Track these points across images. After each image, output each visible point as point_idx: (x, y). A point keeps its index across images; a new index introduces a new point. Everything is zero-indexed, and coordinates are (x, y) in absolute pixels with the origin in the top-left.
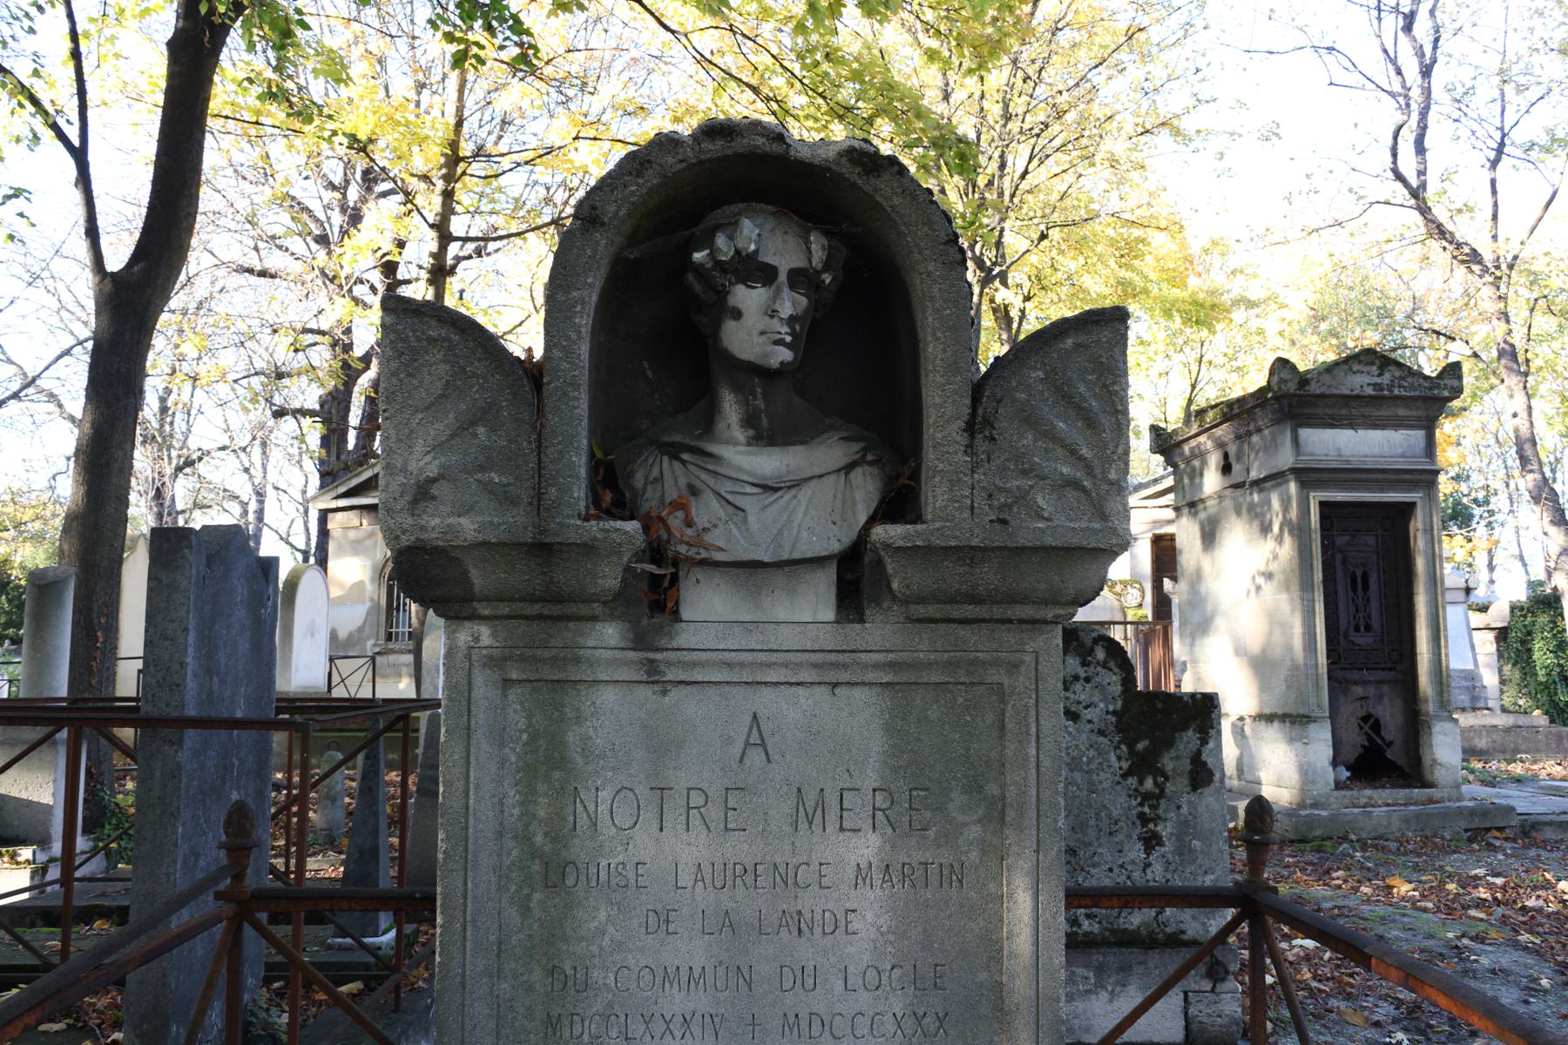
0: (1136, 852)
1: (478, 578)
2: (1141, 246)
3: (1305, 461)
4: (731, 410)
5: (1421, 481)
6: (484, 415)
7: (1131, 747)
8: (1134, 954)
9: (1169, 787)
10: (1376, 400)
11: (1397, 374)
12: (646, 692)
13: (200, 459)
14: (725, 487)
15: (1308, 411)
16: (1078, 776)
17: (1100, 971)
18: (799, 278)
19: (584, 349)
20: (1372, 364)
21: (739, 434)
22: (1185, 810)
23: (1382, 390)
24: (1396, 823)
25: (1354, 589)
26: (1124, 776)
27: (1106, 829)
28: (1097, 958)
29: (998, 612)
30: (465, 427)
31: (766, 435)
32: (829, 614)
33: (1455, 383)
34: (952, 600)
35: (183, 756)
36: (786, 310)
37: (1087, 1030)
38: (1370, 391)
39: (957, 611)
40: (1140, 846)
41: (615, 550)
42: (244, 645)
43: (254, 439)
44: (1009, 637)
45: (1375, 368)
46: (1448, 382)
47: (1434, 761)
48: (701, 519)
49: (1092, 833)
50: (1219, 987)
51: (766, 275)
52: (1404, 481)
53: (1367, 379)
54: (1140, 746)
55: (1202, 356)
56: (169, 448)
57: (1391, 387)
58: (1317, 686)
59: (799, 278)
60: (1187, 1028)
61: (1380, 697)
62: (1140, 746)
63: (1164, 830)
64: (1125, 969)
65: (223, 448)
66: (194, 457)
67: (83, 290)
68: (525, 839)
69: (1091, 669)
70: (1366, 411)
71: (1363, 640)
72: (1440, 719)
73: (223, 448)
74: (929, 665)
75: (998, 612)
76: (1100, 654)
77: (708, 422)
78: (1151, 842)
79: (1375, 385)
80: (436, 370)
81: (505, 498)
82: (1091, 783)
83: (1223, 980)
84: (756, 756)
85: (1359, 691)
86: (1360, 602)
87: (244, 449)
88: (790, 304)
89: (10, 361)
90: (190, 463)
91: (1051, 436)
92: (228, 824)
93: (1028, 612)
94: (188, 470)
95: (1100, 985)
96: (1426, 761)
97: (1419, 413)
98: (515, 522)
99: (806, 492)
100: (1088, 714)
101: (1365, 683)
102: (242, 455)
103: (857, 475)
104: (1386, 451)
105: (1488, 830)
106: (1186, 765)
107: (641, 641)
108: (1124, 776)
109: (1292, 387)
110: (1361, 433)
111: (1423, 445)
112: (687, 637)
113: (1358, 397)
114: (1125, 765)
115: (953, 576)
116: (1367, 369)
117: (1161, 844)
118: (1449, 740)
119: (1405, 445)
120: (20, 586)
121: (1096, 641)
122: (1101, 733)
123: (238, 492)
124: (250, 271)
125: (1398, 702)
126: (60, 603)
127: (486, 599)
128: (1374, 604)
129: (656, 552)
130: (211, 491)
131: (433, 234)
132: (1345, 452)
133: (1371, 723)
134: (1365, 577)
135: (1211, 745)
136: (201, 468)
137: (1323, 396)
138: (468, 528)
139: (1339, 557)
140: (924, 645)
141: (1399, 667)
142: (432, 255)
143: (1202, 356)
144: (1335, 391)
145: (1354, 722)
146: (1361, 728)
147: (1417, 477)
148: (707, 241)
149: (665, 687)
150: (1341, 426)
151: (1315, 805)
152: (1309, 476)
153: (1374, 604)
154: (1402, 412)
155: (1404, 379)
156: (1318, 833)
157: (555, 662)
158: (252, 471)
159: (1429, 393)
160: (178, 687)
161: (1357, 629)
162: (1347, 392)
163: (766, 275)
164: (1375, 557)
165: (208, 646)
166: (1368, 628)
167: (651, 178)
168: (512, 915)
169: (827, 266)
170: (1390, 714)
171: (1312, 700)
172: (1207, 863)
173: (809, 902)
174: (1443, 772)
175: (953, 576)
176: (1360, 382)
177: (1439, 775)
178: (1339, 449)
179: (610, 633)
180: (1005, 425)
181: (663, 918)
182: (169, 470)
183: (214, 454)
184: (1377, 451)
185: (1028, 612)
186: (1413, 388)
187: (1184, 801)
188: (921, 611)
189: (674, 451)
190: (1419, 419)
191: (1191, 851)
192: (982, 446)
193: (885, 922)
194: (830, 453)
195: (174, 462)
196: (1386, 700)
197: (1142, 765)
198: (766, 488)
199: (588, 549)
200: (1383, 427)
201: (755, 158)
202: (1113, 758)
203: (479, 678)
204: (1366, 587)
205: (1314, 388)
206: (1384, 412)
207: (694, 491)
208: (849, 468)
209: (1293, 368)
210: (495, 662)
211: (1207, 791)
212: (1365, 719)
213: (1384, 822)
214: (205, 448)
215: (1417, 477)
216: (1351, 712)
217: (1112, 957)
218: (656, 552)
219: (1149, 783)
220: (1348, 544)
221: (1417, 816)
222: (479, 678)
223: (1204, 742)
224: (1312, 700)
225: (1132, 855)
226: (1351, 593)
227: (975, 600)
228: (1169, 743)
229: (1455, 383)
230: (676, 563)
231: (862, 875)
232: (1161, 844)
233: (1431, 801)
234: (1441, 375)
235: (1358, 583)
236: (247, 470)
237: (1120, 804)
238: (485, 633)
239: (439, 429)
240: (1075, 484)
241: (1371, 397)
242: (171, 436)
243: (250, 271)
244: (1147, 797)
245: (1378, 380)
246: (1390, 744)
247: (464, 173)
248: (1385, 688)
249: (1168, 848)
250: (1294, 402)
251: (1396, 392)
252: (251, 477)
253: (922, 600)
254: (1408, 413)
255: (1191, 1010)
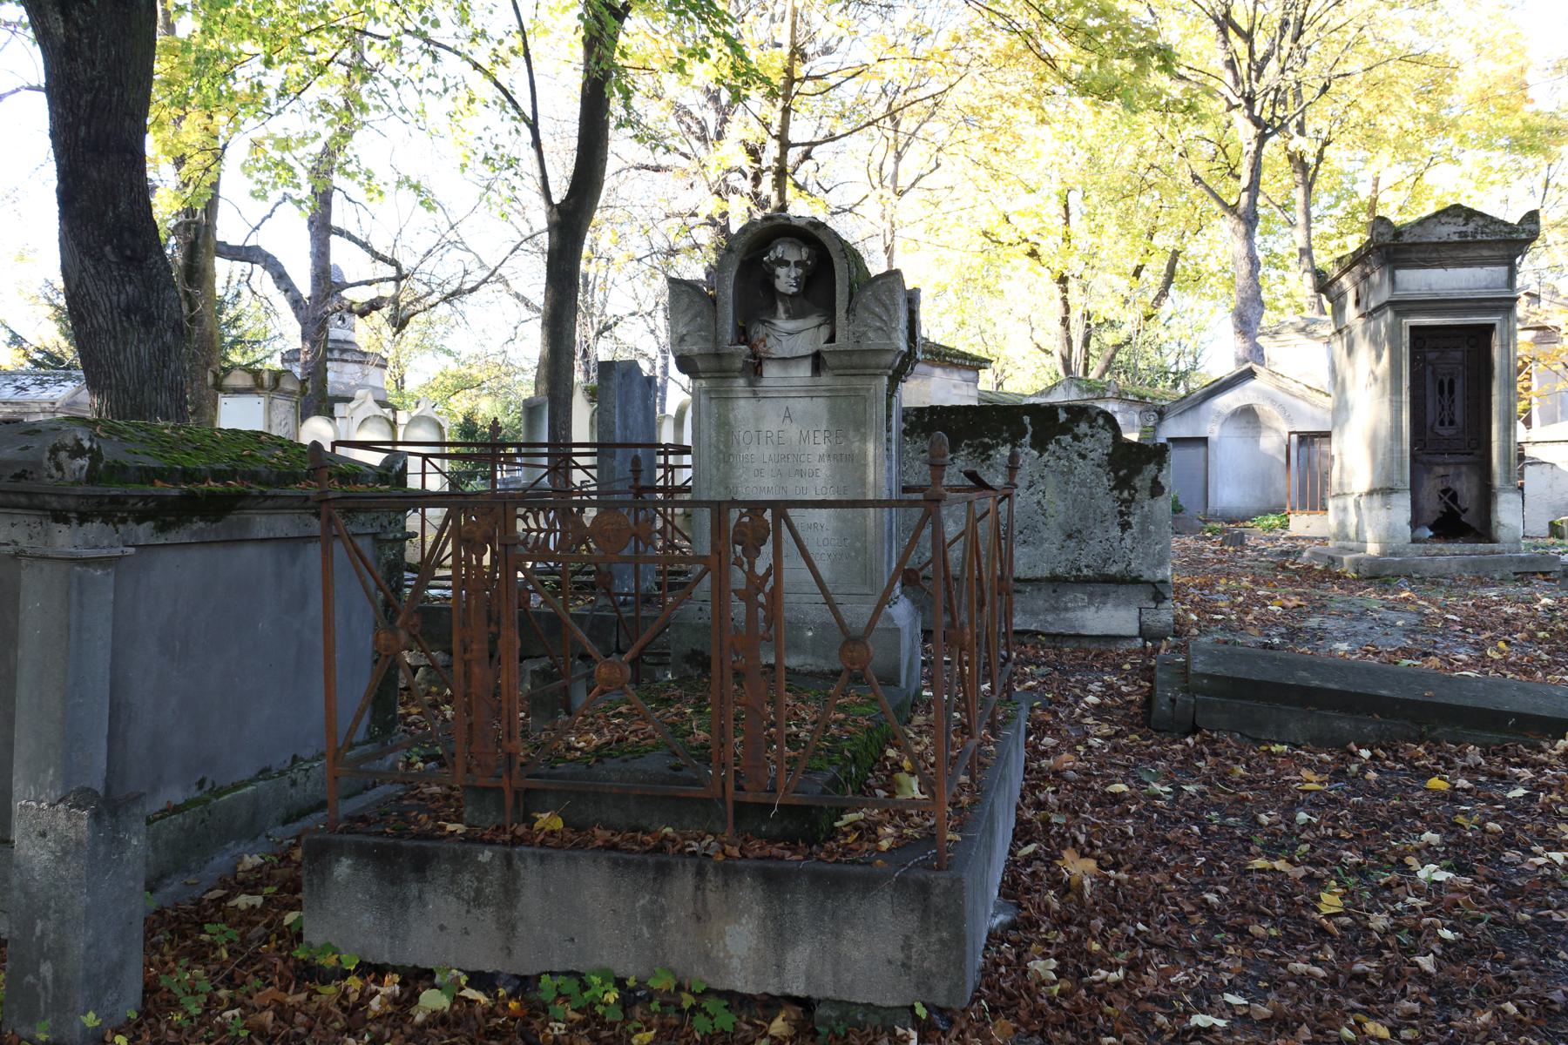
0: (1117, 532)
1: (700, 365)
2: (1447, 80)
3: (1400, 295)
4: (781, 308)
5: (1501, 307)
6: (699, 314)
7: (1116, 473)
8: (1112, 587)
9: (1137, 496)
10: (1463, 244)
11: (1481, 223)
12: (753, 401)
13: (616, 324)
14: (777, 334)
15: (1403, 256)
16: (1084, 490)
17: (1091, 595)
18: (797, 264)
19: (730, 292)
20: (1460, 216)
21: (783, 316)
22: (1146, 509)
23: (1466, 236)
24: (1454, 567)
25: (1441, 392)
26: (1111, 490)
27: (1099, 519)
28: (1090, 588)
29: (861, 372)
30: (694, 318)
31: (792, 316)
32: (809, 374)
33: (1533, 227)
34: (846, 368)
35: (616, 463)
36: (793, 275)
37: (1083, 627)
38: (1455, 238)
39: (848, 372)
40: (1118, 528)
41: (740, 355)
42: (640, 418)
43: (657, 304)
44: (867, 381)
45: (1461, 219)
46: (1527, 227)
47: (1499, 523)
48: (769, 345)
49: (1091, 521)
50: (1160, 606)
51: (787, 264)
52: (1486, 307)
53: (1453, 229)
54: (1121, 473)
55: (1548, 181)
56: (592, 315)
57: (1474, 234)
58: (1401, 466)
59: (797, 264)
60: (1140, 628)
61: (1459, 475)
62: (1121, 473)
63: (1133, 520)
64: (1106, 595)
65: (633, 314)
66: (611, 322)
67: (540, 220)
68: (717, 448)
69: (1095, 430)
70: (1454, 254)
71: (1446, 432)
72: (1505, 491)
73: (633, 314)
74: (841, 390)
75: (861, 372)
76: (1101, 421)
77: (774, 314)
78: (1125, 526)
79: (1460, 233)
80: (685, 300)
81: (706, 339)
82: (1091, 494)
83: (1162, 602)
84: (788, 420)
85: (1441, 470)
86: (1446, 403)
87: (650, 314)
88: (795, 272)
89: (468, 250)
90: (607, 328)
91: (874, 313)
92: (633, 462)
93: (871, 371)
94: (605, 334)
95: (1091, 603)
96: (1494, 524)
97: (1502, 253)
98: (707, 347)
99: (803, 334)
100: (1091, 455)
101: (1446, 464)
102: (648, 318)
103: (822, 328)
104: (1471, 284)
105: (1534, 573)
106: (1149, 483)
107: (751, 384)
108: (1111, 490)
109: (1387, 239)
110: (1451, 271)
111: (1505, 278)
112: (764, 382)
113: (1445, 243)
114: (1112, 484)
115: (845, 360)
116: (1455, 220)
117: (1131, 527)
118: (1512, 507)
119: (1489, 279)
120: (484, 433)
121: (1098, 414)
122: (1099, 466)
123: (646, 352)
124: (647, 167)
125: (1475, 479)
126: (541, 419)
127: (703, 372)
128: (1459, 403)
129: (754, 355)
130: (624, 350)
131: (776, 143)
132: (1436, 287)
133: (1450, 495)
134: (1451, 383)
135: (1164, 472)
136: (617, 331)
137: (1414, 244)
138: (695, 349)
139: (1430, 368)
140: (839, 383)
141: (1476, 452)
142: (776, 160)
143: (1548, 181)
144: (1424, 240)
145: (1435, 494)
146: (1441, 498)
147: (1497, 304)
148: (767, 253)
149: (759, 399)
150: (1433, 267)
151: (1394, 554)
152: (1401, 307)
153: (1459, 403)
154: (1486, 253)
155: (1486, 227)
156: (1389, 572)
157: (725, 392)
158: (657, 332)
159: (1508, 237)
160: (612, 432)
161: (1442, 423)
162: (1436, 240)
163: (787, 264)
164: (1461, 368)
165: (625, 415)
166: (1452, 423)
167: (749, 235)
168: (714, 471)
169: (808, 259)
170: (1466, 488)
171: (1396, 477)
172: (1158, 538)
173: (805, 466)
174: (1505, 530)
175: (845, 360)
176: (1448, 231)
177: (1502, 533)
178: (1430, 285)
179: (741, 382)
180: (859, 310)
181: (760, 472)
182: (592, 334)
183: (626, 319)
184: (1463, 285)
185: (871, 371)
186: (1494, 233)
187: (1146, 504)
188: (837, 372)
189: (763, 322)
190: (1502, 257)
191: (1148, 532)
192: (851, 317)
193: (828, 473)
194: (813, 321)
195: (596, 326)
196: (1464, 477)
197: (1122, 483)
198: (789, 334)
199: (731, 355)
200: (1470, 265)
201: (780, 225)
202: (1105, 479)
203: (702, 397)
204: (1451, 391)
205: (1407, 239)
206: (1470, 254)
207: (767, 335)
208: (819, 326)
209: (1390, 224)
210: (707, 392)
211: (1160, 498)
212: (1445, 492)
213: (1445, 566)
214: (619, 315)
215: (1497, 304)
216: (1431, 487)
217: (1098, 589)
218: (754, 355)
219: (1126, 494)
220: (1437, 358)
221: (1473, 562)
222: (702, 397)
223: (1160, 470)
224: (1396, 477)
225: (1113, 534)
226: (1438, 397)
227: (853, 368)
228: (1139, 471)
229: (1533, 227)
230: (761, 359)
231: (821, 458)
232: (1131, 527)
233: (1493, 552)
234: (1520, 223)
235: (1446, 388)
236: (652, 332)
237: (1108, 505)
238: (703, 383)
239: (687, 319)
240: (881, 329)
241: (1455, 242)
242: (592, 305)
243: (647, 167)
244: (1124, 501)
245: (1464, 229)
246: (1465, 511)
247: (797, 93)
248: (1464, 469)
249: (1135, 530)
250: (1392, 249)
251: (1479, 237)
252: (657, 337)
253: (837, 368)
254: (1492, 253)
255: (1143, 618)
